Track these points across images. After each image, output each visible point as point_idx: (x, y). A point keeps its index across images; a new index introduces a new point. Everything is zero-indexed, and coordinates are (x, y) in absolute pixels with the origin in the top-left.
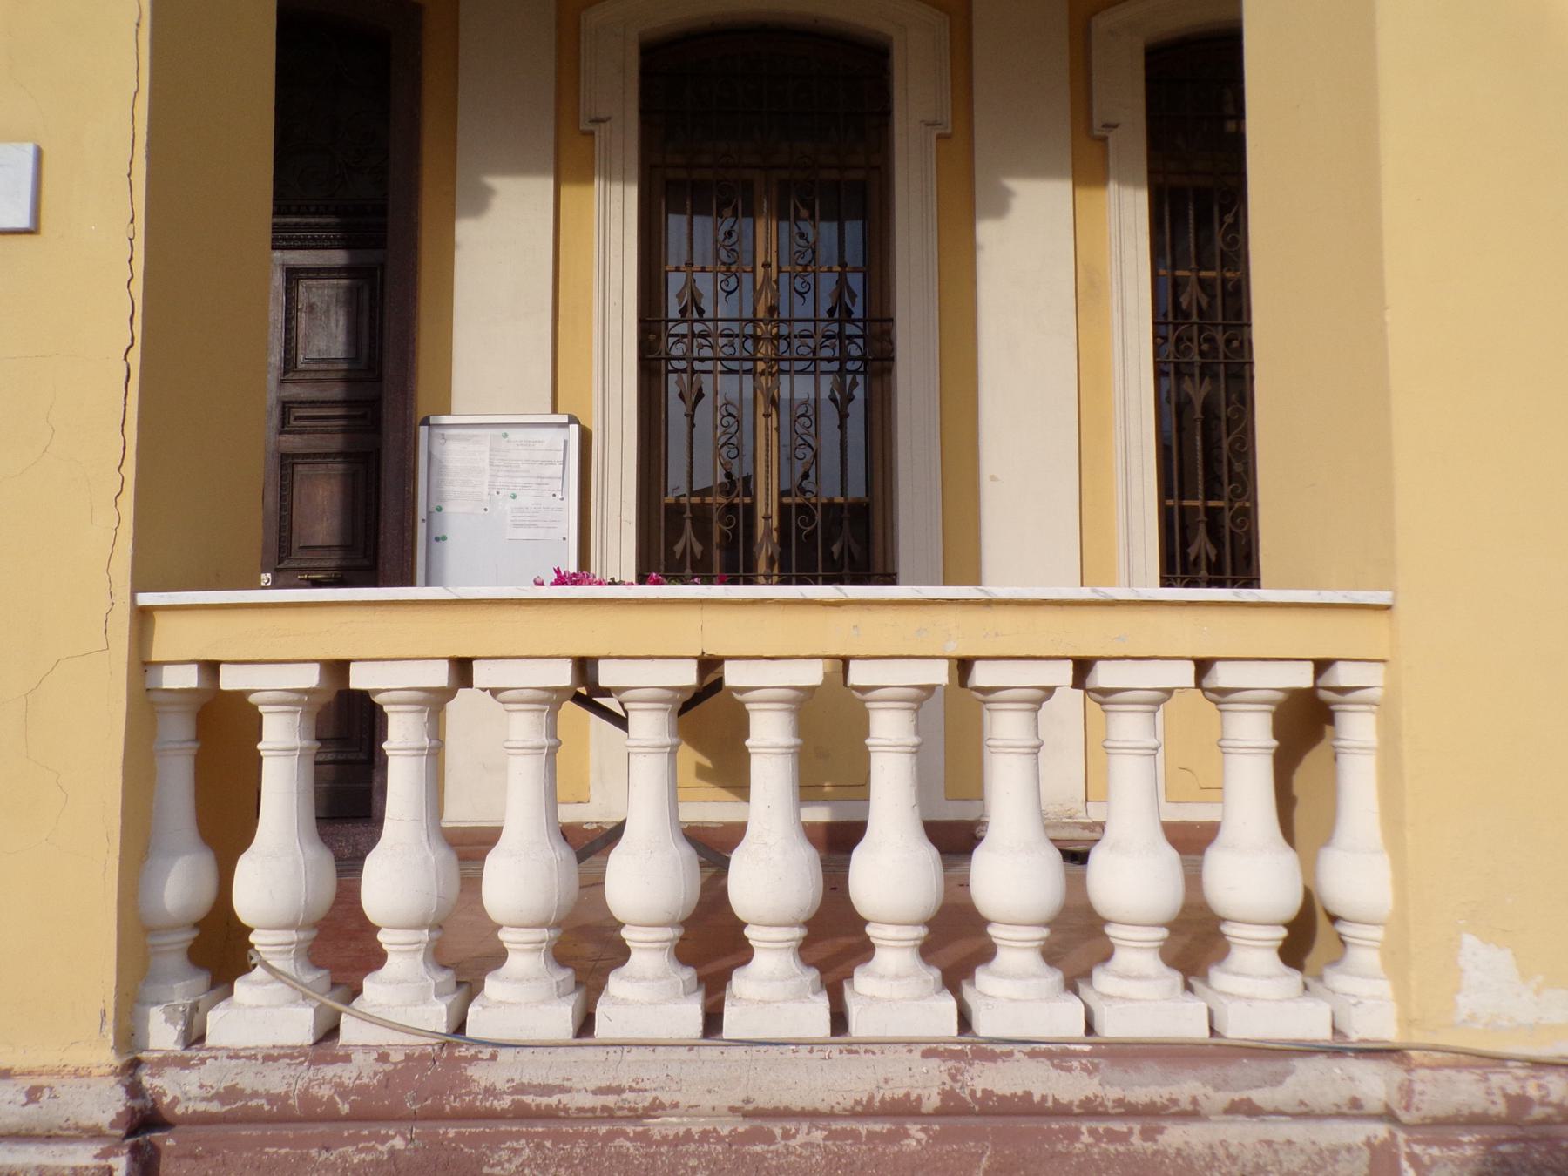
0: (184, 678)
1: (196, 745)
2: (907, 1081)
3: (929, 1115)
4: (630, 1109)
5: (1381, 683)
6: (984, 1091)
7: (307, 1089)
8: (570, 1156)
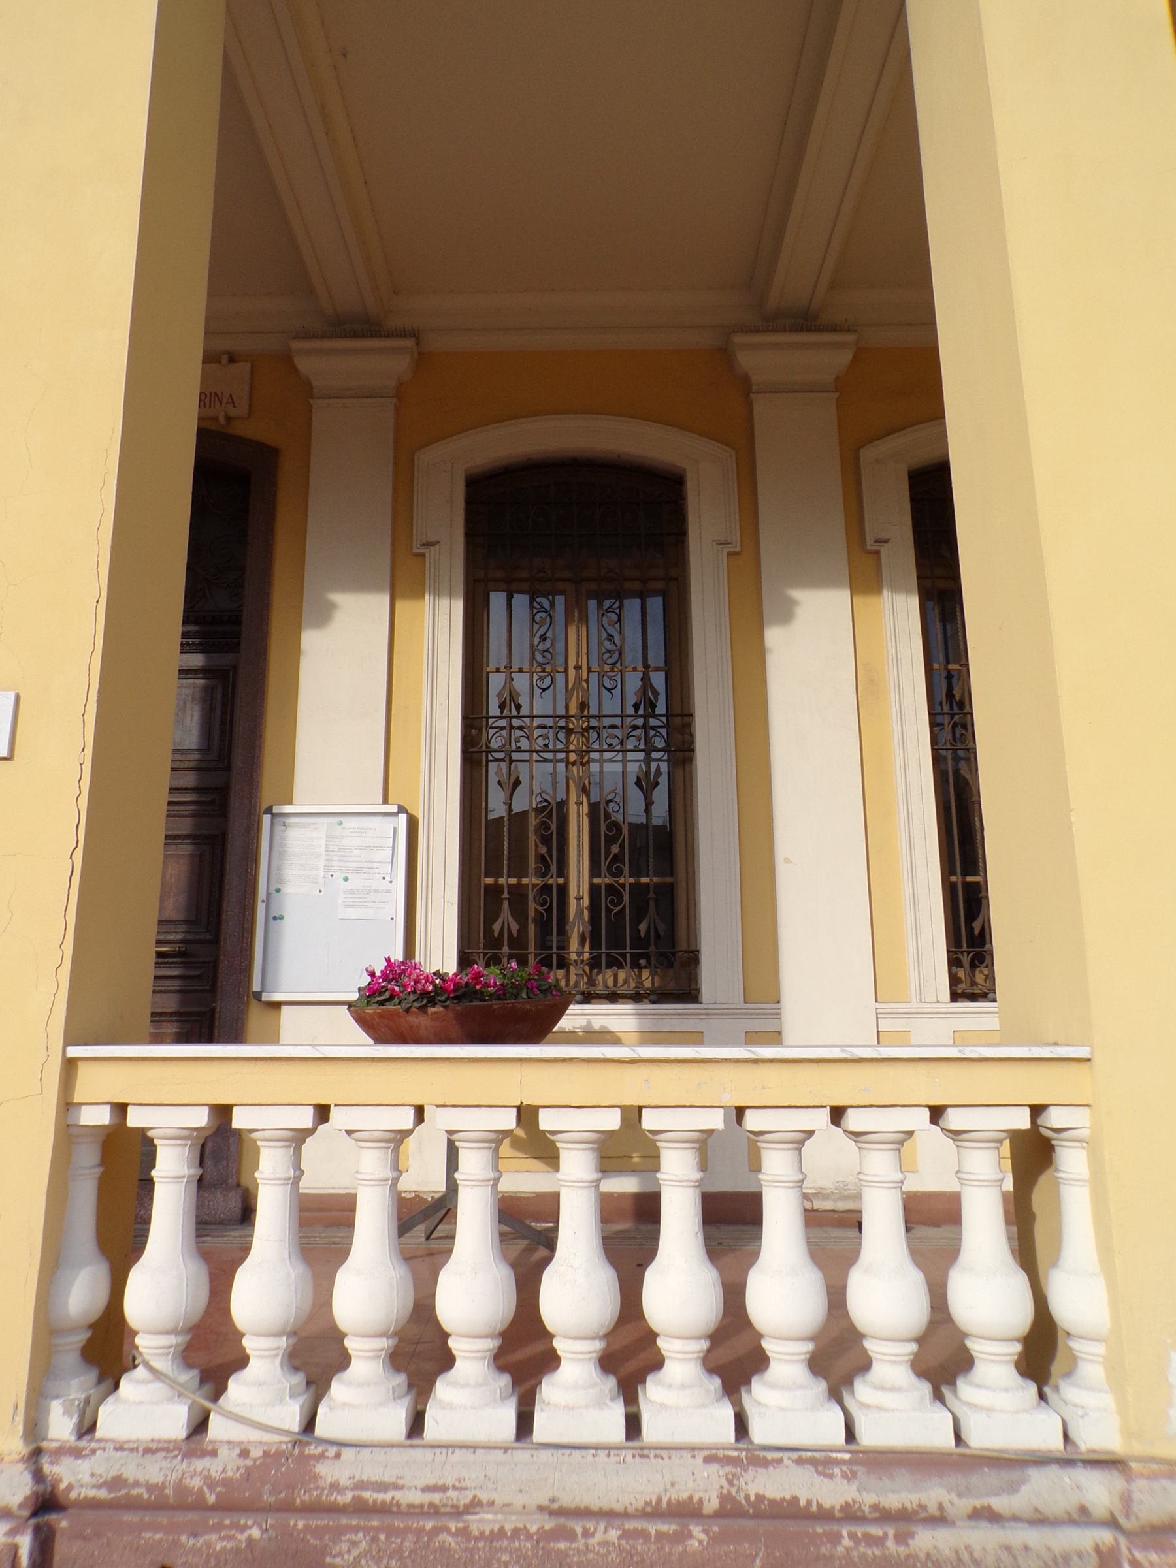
0: (101, 1117)
1: (99, 1170)
2: (690, 1484)
3: (709, 1517)
4: (453, 1506)
5: (1088, 1125)
6: (757, 1495)
7: (181, 1480)
8: (400, 1549)
